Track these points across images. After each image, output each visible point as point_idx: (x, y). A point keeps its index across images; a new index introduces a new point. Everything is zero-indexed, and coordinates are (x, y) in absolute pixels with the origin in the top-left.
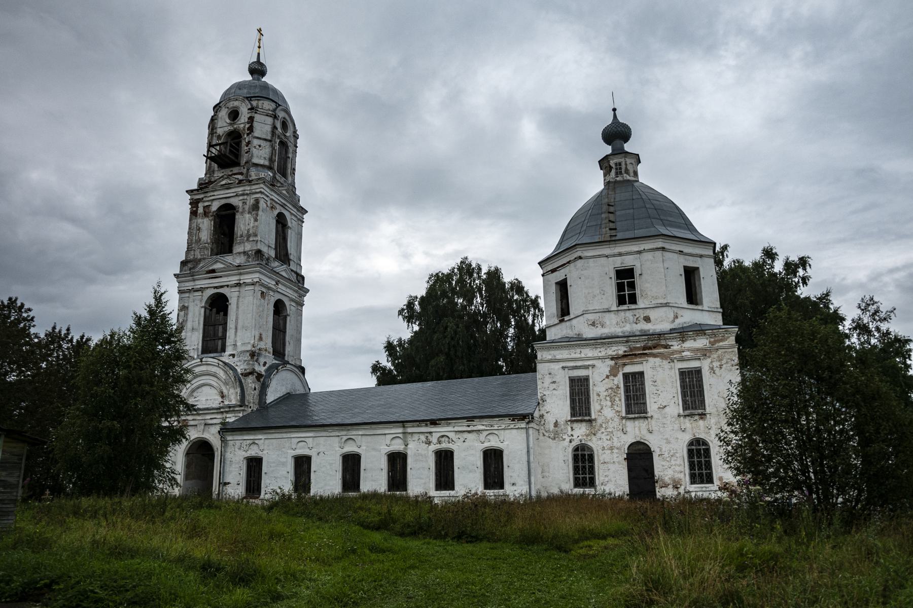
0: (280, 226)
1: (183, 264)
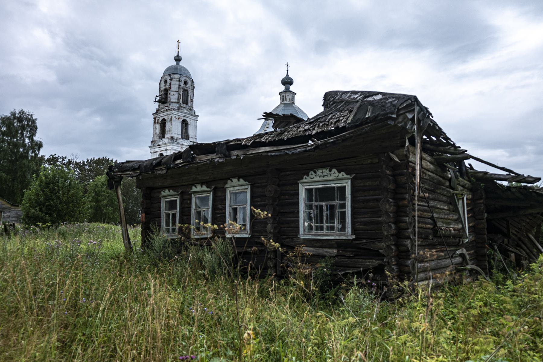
0: (184, 125)
1: (152, 142)
